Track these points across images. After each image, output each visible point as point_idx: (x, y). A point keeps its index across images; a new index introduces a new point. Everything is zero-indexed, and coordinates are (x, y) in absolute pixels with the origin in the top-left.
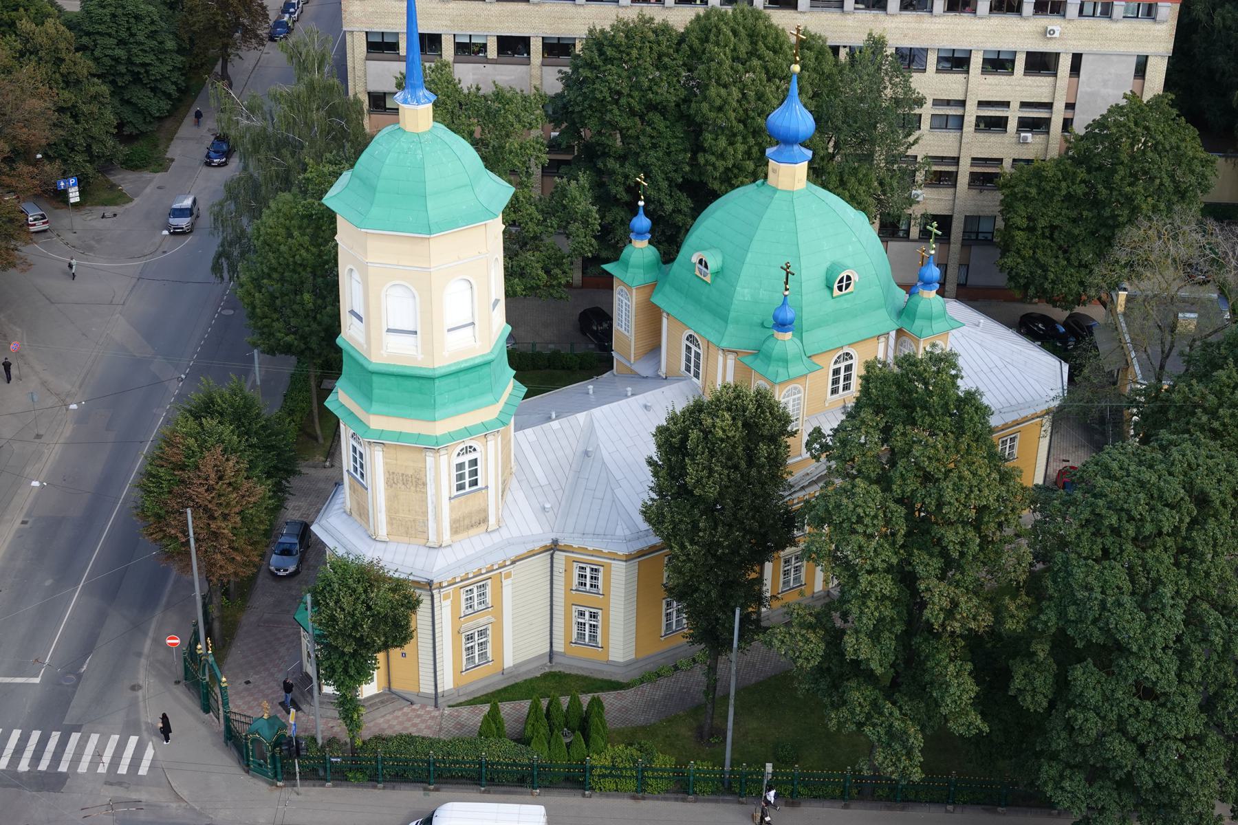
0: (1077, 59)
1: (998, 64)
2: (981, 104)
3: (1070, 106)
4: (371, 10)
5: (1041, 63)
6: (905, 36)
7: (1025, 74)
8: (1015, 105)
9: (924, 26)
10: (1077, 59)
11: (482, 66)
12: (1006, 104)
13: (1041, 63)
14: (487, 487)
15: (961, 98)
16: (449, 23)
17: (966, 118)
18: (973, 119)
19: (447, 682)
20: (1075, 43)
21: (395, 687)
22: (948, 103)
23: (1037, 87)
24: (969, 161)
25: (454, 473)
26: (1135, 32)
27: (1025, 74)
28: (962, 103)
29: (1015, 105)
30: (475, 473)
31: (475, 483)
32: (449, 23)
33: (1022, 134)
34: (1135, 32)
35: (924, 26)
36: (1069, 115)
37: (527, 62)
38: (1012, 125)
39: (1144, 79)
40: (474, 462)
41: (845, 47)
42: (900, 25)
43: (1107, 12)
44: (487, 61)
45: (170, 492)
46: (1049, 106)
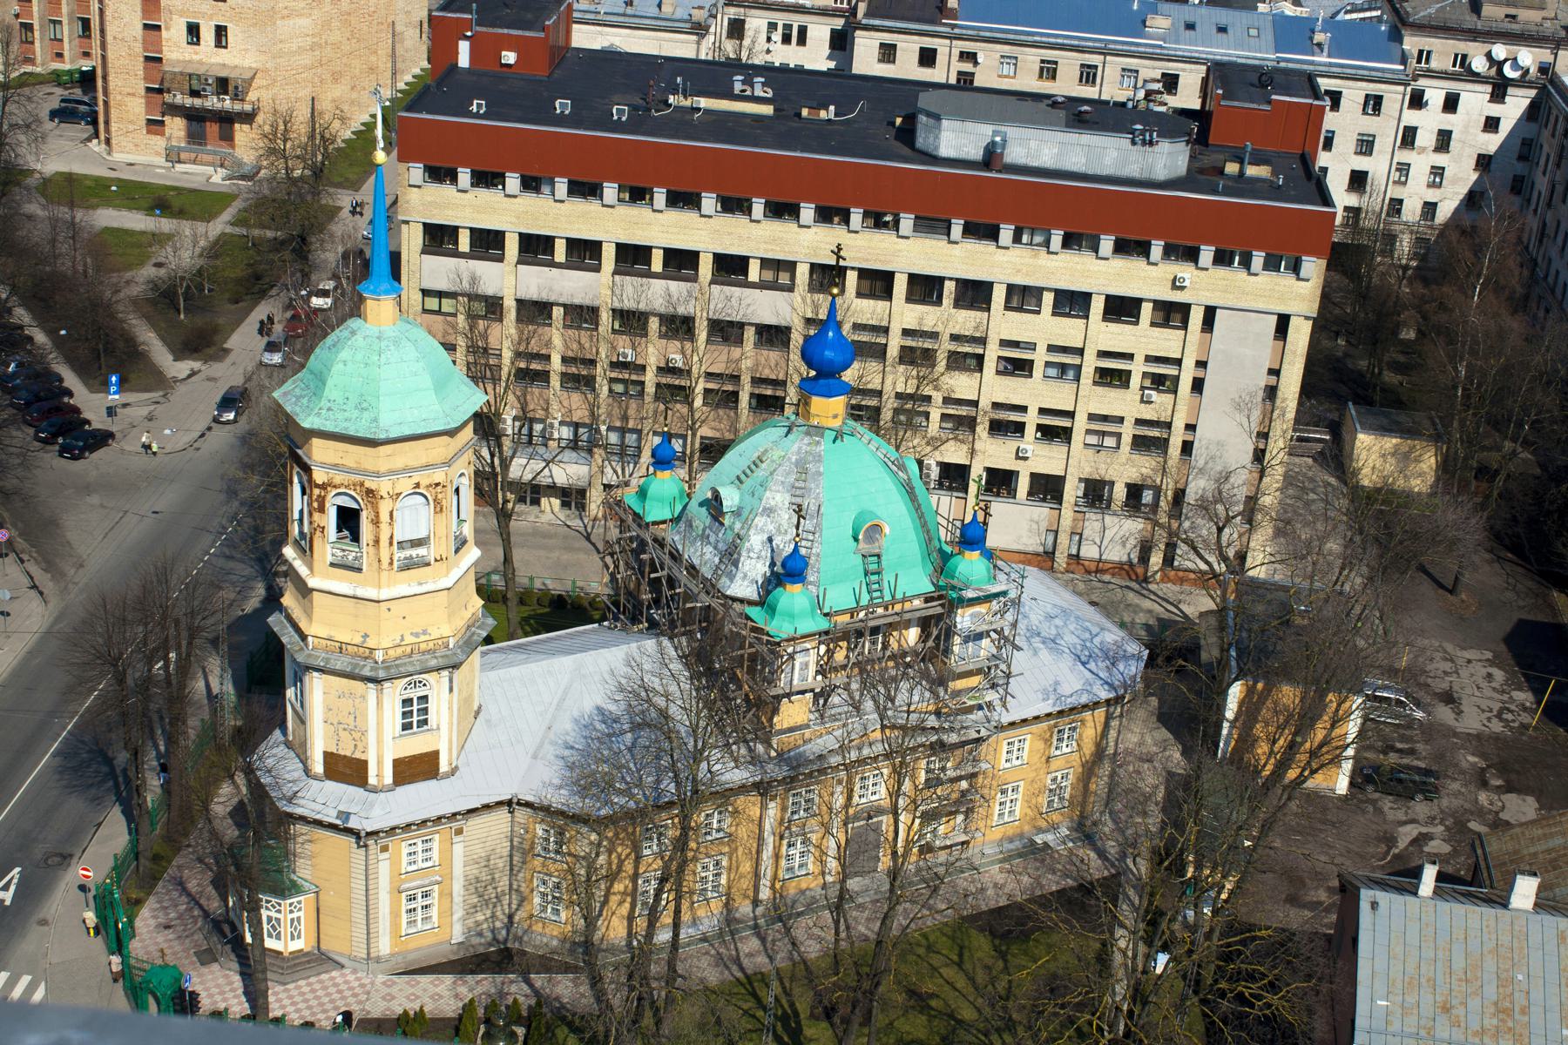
0: (1210, 313)
1: (1122, 309)
2: (1103, 354)
3: (1202, 364)
4: (429, 198)
5: (1172, 314)
6: (1019, 271)
7: (1105, 319)
8: (1139, 358)
9: (1040, 262)
10: (1210, 313)
11: (547, 269)
12: (1130, 357)
13: (1172, 314)
14: (438, 728)
15: (1080, 345)
16: (514, 220)
17: (986, 358)
18: (1092, 370)
19: (384, 946)
20: (1207, 294)
21: (323, 947)
22: (1064, 350)
23: (1167, 341)
24: (1086, 416)
25: (399, 710)
26: (1277, 288)
27: (1105, 319)
28: (1080, 352)
29: (1139, 358)
30: (425, 711)
31: (425, 722)
32: (514, 220)
33: (1146, 392)
34: (1277, 288)
35: (1040, 262)
36: (1200, 374)
37: (694, 279)
38: (1135, 381)
39: (1285, 341)
40: (424, 699)
41: (951, 279)
42: (1013, 259)
43: (1246, 263)
44: (456, 254)
45: (557, 852)
46: (1178, 362)
